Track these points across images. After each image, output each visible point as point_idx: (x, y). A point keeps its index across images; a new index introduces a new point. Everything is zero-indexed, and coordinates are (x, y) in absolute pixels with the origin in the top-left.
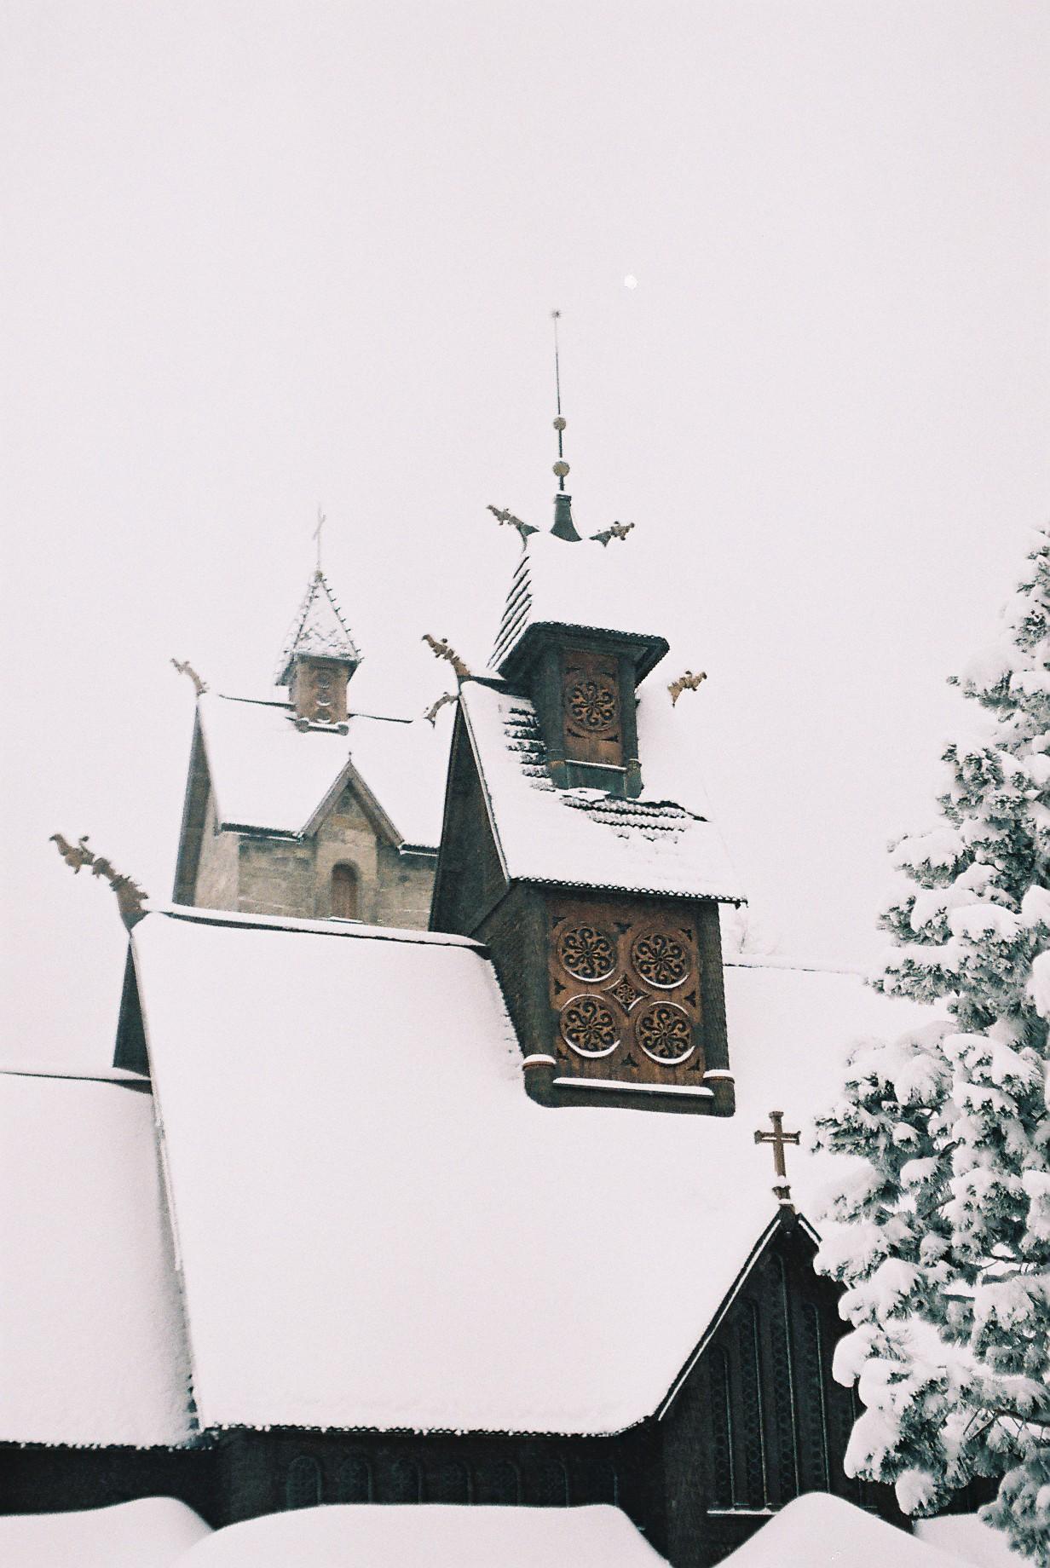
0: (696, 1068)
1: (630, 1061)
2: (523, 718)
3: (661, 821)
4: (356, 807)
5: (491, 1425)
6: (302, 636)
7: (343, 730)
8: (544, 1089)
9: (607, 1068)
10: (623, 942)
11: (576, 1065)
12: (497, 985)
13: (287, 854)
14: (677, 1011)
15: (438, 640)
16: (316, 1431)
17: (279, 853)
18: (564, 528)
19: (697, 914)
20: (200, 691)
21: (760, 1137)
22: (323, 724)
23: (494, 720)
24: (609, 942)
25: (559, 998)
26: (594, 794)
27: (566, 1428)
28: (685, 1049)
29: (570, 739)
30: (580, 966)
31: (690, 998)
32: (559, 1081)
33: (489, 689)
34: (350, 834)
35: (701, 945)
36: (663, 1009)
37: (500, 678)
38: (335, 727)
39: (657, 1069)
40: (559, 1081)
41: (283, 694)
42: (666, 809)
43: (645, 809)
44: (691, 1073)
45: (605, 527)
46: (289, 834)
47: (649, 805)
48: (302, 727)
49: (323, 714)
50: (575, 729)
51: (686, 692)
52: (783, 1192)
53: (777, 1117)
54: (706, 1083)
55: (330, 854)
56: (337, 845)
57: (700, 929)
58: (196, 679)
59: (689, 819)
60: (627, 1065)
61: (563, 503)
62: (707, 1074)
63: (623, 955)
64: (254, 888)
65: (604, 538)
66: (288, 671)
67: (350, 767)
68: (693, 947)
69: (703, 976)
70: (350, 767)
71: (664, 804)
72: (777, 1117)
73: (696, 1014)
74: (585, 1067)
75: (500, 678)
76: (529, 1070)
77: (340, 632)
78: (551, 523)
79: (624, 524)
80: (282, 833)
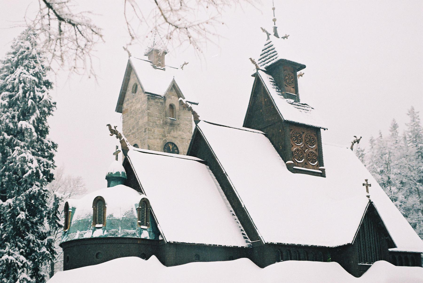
0: (318, 166)
1: (306, 164)
2: (272, 80)
3: (306, 108)
4: (174, 90)
5: (315, 244)
6: (155, 44)
7: (164, 69)
8: (292, 169)
9: (302, 165)
10: (303, 136)
11: (296, 164)
12: (271, 143)
13: (158, 101)
14: (314, 153)
15: (253, 59)
16: (285, 244)
17: (156, 100)
18: (276, 35)
19: (317, 130)
20: (130, 56)
21: (364, 185)
22: (160, 67)
23: (267, 80)
24: (301, 136)
25: (292, 148)
26: (292, 101)
27: (327, 245)
28: (316, 162)
29: (286, 87)
30: (296, 141)
31: (316, 150)
32: (294, 167)
33: (263, 72)
34: (173, 97)
35: (317, 138)
36: (311, 152)
37: (265, 70)
38: (162, 68)
39: (311, 166)
40: (294, 167)
41: (147, 58)
42: (306, 106)
43: (302, 105)
44: (317, 167)
45: (284, 36)
46: (160, 96)
47: (302, 104)
48: (155, 67)
49: (159, 65)
50: (286, 85)
51: (301, 77)
52: (368, 197)
53: (366, 180)
54: (319, 169)
55: (169, 102)
56: (170, 99)
57: (317, 134)
58: (129, 52)
59: (311, 108)
60: (305, 165)
61: (275, 28)
62: (320, 168)
63: (303, 139)
64: (151, 109)
65: (284, 38)
66: (149, 53)
67: (174, 81)
68: (316, 138)
69: (318, 145)
70: (174, 81)
71: (305, 104)
72: (366, 180)
73: (317, 154)
74: (298, 165)
75: (265, 70)
76: (323, 166)
77: (163, 44)
78: (274, 33)
79: (288, 35)
80: (158, 95)
